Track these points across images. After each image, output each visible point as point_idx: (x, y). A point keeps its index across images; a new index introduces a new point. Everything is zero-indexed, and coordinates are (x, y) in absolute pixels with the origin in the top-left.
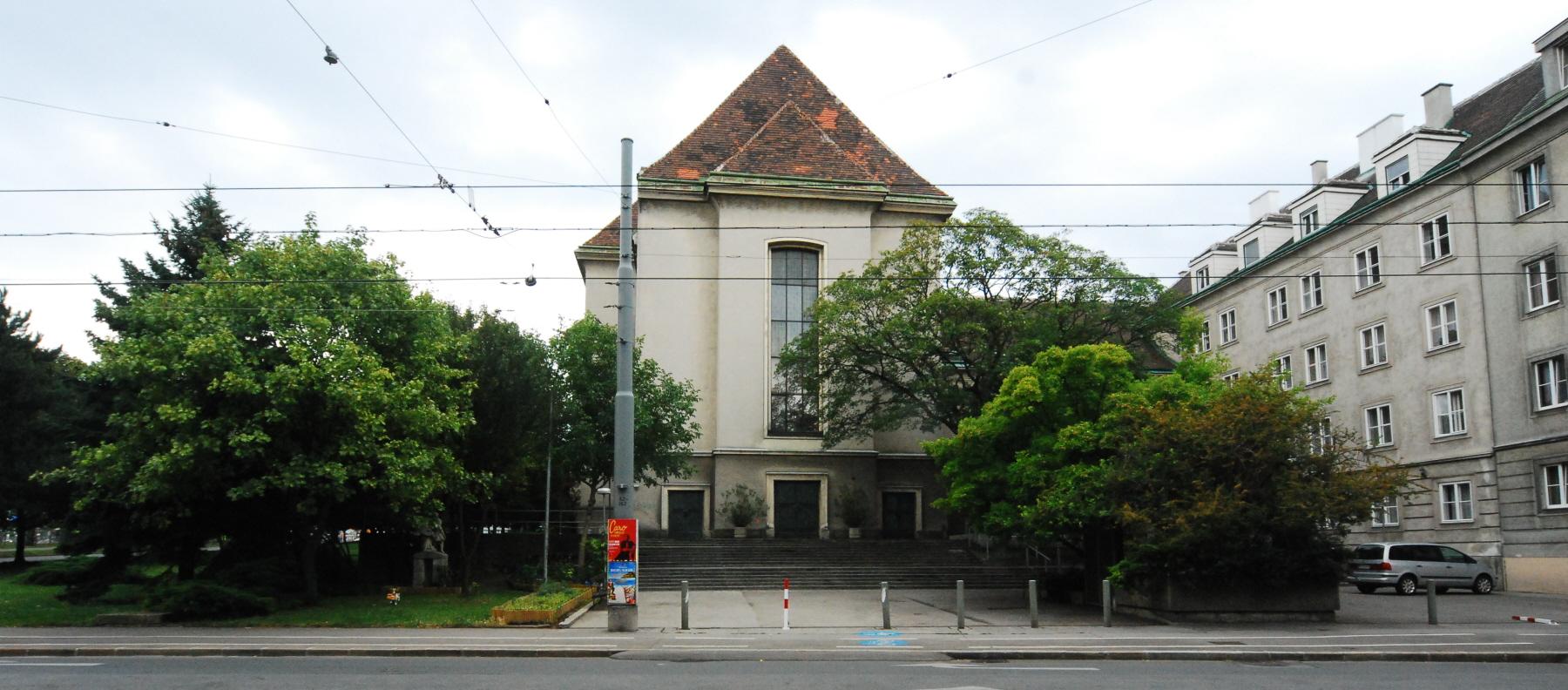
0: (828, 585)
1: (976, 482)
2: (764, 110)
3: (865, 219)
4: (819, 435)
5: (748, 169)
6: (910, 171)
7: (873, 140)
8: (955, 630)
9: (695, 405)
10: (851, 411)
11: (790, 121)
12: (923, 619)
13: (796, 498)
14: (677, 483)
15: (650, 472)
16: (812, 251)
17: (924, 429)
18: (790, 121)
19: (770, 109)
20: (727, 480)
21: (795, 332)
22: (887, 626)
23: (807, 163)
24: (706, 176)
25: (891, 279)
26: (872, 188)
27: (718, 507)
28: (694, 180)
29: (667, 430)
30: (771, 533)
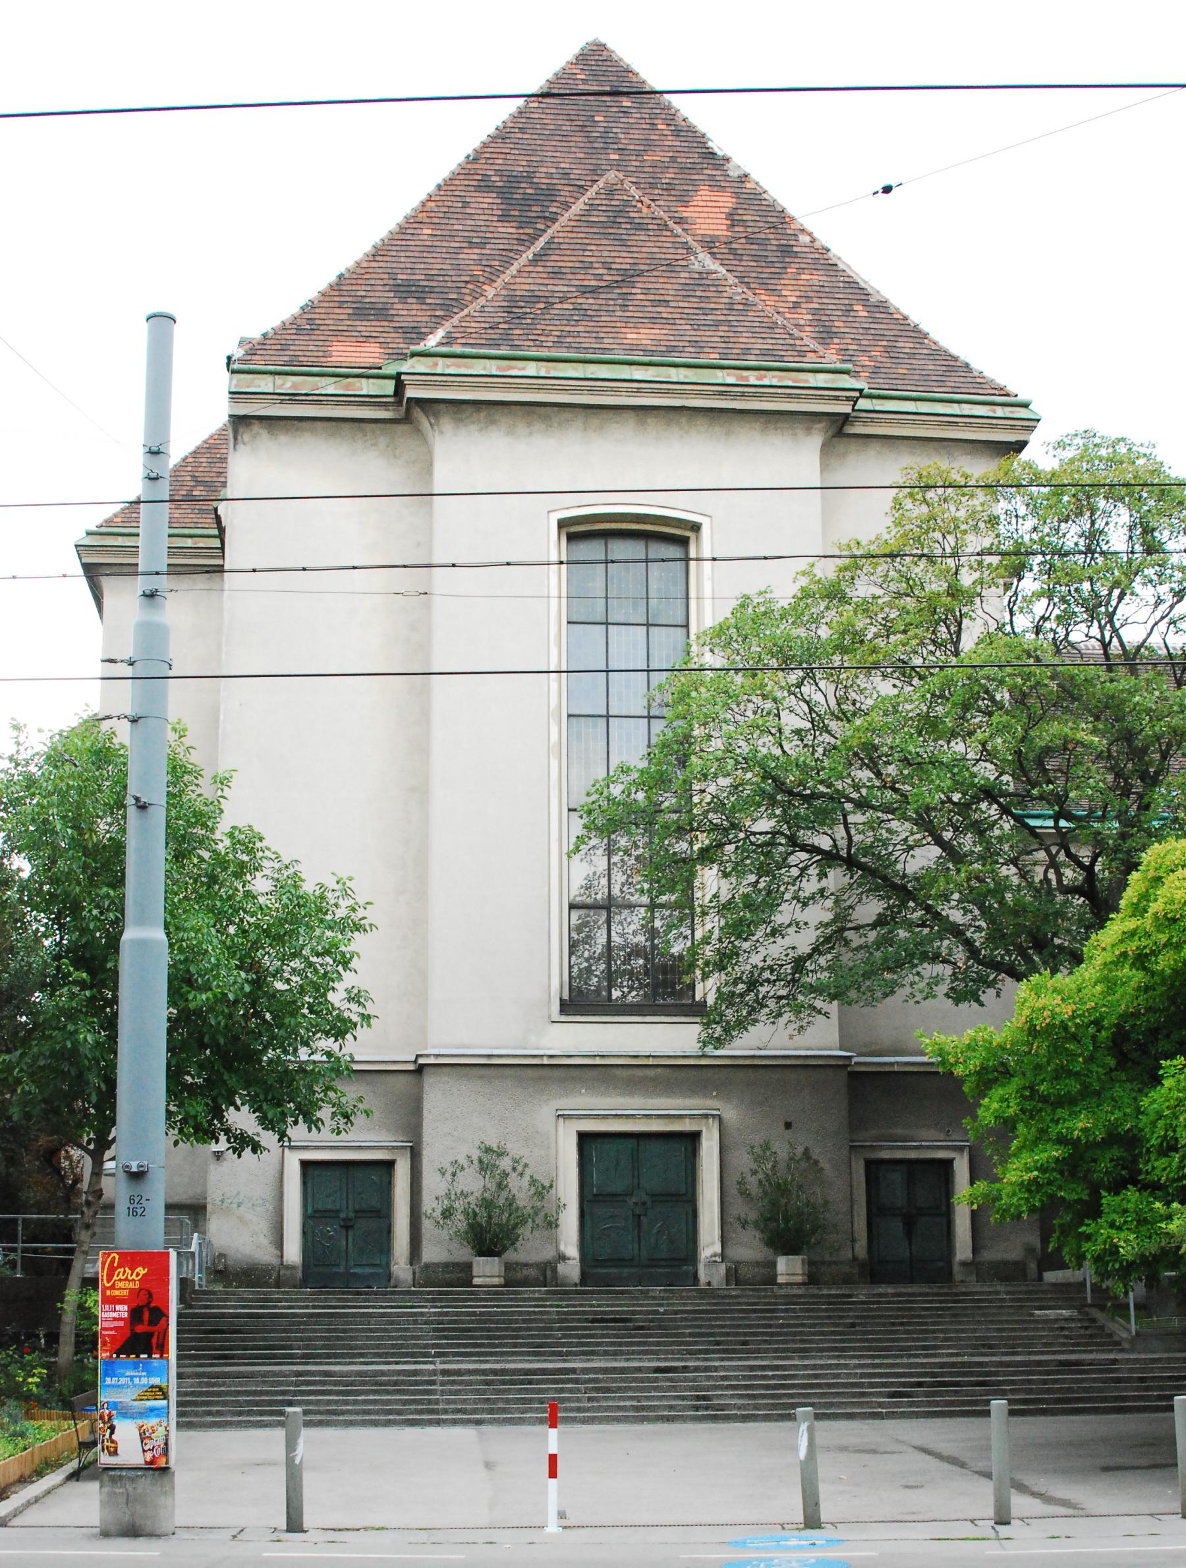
0: (706, 1409)
1: (1061, 1140)
2: (549, 194)
3: (810, 446)
4: (697, 1010)
5: (506, 339)
6: (919, 335)
7: (823, 260)
8: (986, 1528)
9: (358, 943)
10: (775, 950)
11: (615, 219)
12: (920, 1500)
13: (635, 1180)
14: (322, 1141)
15: (242, 1118)
16: (671, 537)
17: (957, 996)
18: (615, 219)
19: (565, 193)
20: (456, 1131)
21: (632, 748)
22: (812, 1521)
23: (654, 320)
24: (403, 357)
25: (865, 608)
26: (821, 380)
27: (428, 1204)
28: (375, 363)
29: (287, 1007)
30: (571, 1270)
